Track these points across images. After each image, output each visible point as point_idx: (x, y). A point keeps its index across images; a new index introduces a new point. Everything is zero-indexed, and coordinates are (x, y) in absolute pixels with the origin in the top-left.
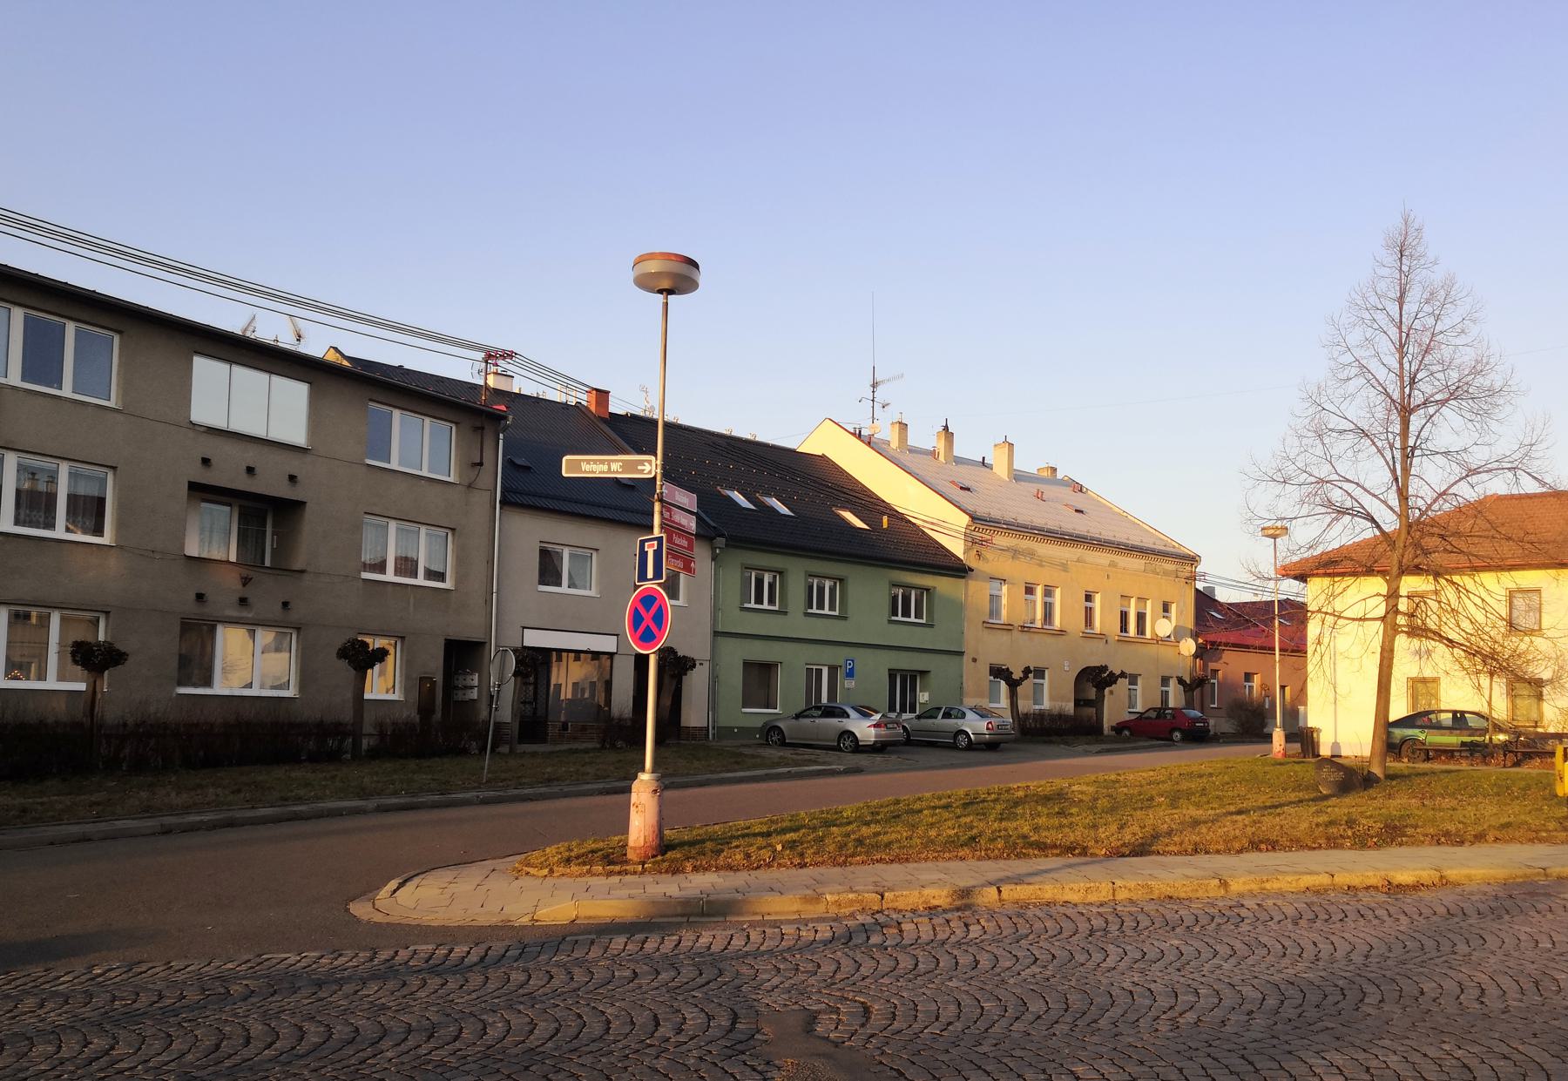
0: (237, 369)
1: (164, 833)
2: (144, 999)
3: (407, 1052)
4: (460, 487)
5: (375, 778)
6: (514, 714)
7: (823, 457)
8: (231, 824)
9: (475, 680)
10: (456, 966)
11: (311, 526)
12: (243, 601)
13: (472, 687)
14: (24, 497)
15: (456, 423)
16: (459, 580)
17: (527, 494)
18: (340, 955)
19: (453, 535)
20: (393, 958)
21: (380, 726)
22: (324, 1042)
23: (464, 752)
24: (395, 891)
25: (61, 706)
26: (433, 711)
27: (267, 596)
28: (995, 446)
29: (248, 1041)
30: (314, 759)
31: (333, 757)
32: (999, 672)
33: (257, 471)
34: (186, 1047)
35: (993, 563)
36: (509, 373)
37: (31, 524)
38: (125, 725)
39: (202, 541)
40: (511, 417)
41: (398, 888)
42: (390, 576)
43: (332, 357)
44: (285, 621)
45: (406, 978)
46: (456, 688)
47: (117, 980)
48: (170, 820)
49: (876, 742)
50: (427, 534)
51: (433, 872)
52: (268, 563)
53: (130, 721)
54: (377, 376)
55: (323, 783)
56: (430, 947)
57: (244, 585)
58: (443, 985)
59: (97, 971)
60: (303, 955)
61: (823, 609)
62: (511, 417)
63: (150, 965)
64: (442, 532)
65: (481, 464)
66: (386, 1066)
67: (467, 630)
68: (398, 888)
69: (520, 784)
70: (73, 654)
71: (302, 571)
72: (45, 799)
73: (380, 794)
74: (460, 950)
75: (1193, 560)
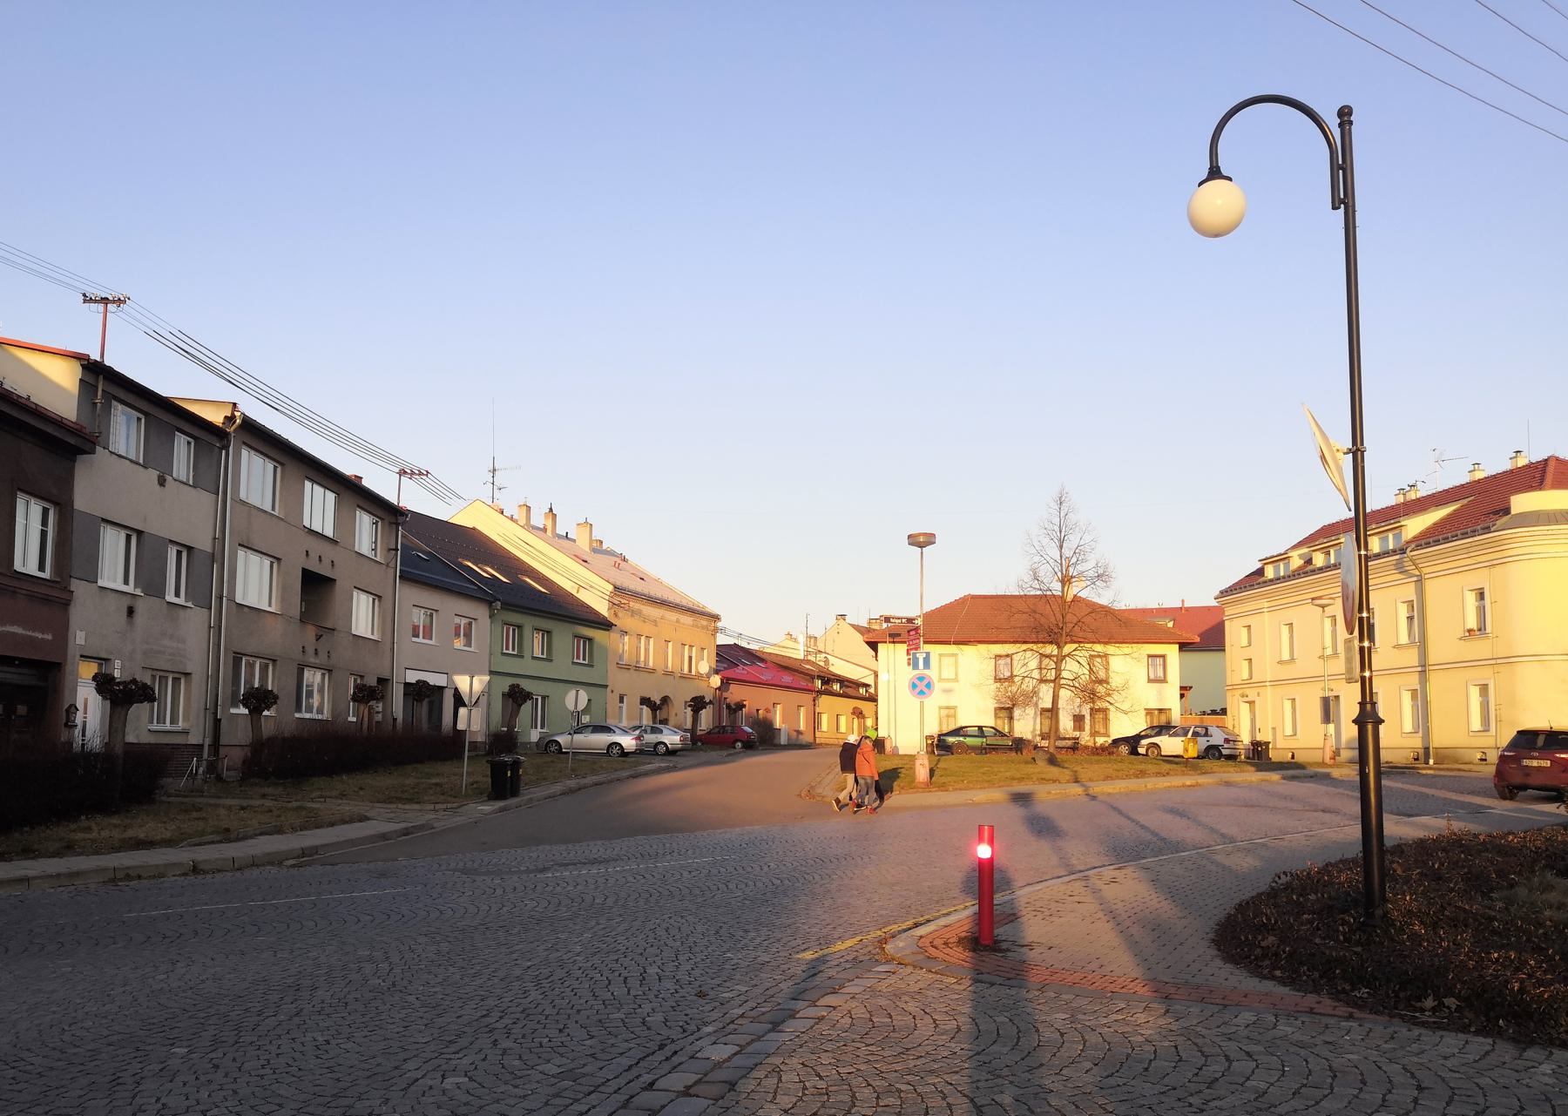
7: (474, 529)
15: (382, 519)
19: (379, 601)
28: (578, 525)
32: (645, 701)
35: (623, 621)
49: (636, 750)
67: (386, 675)
75: (716, 618)
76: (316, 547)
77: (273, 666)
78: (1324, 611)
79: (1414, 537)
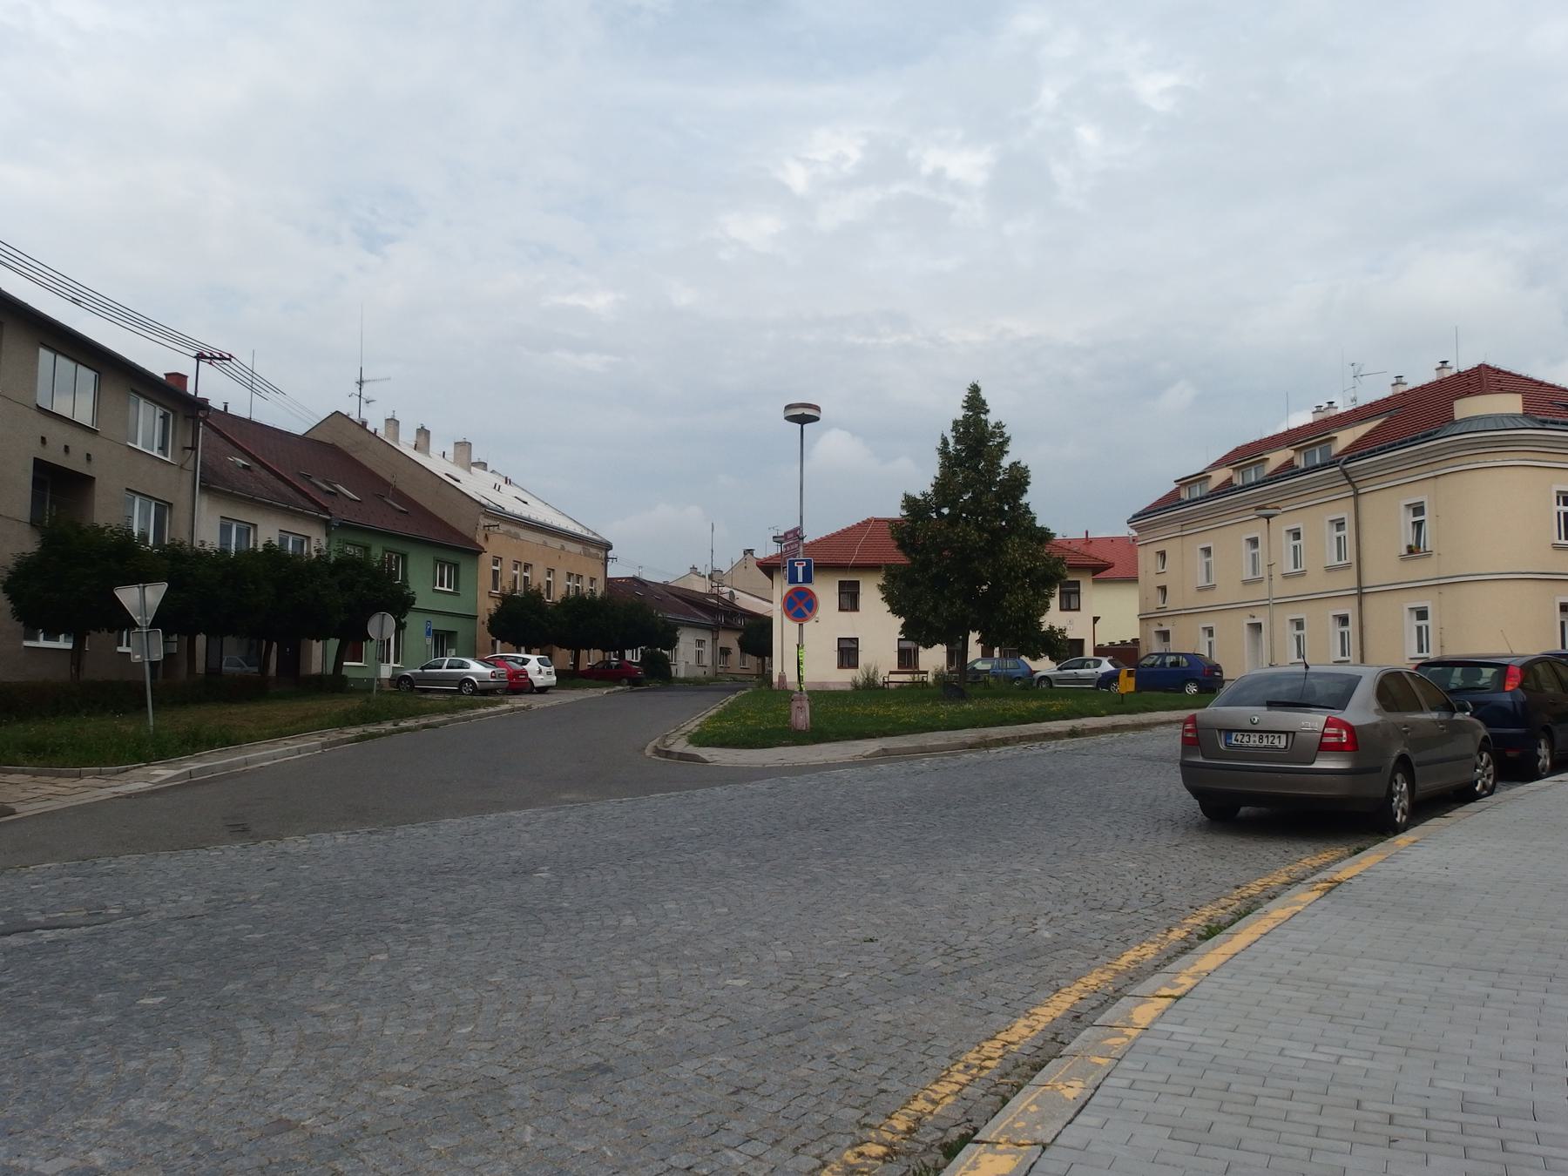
15: (173, 411)
61: (443, 586)
75: (608, 547)
76: (58, 434)
78: (1268, 522)
79: (1344, 450)
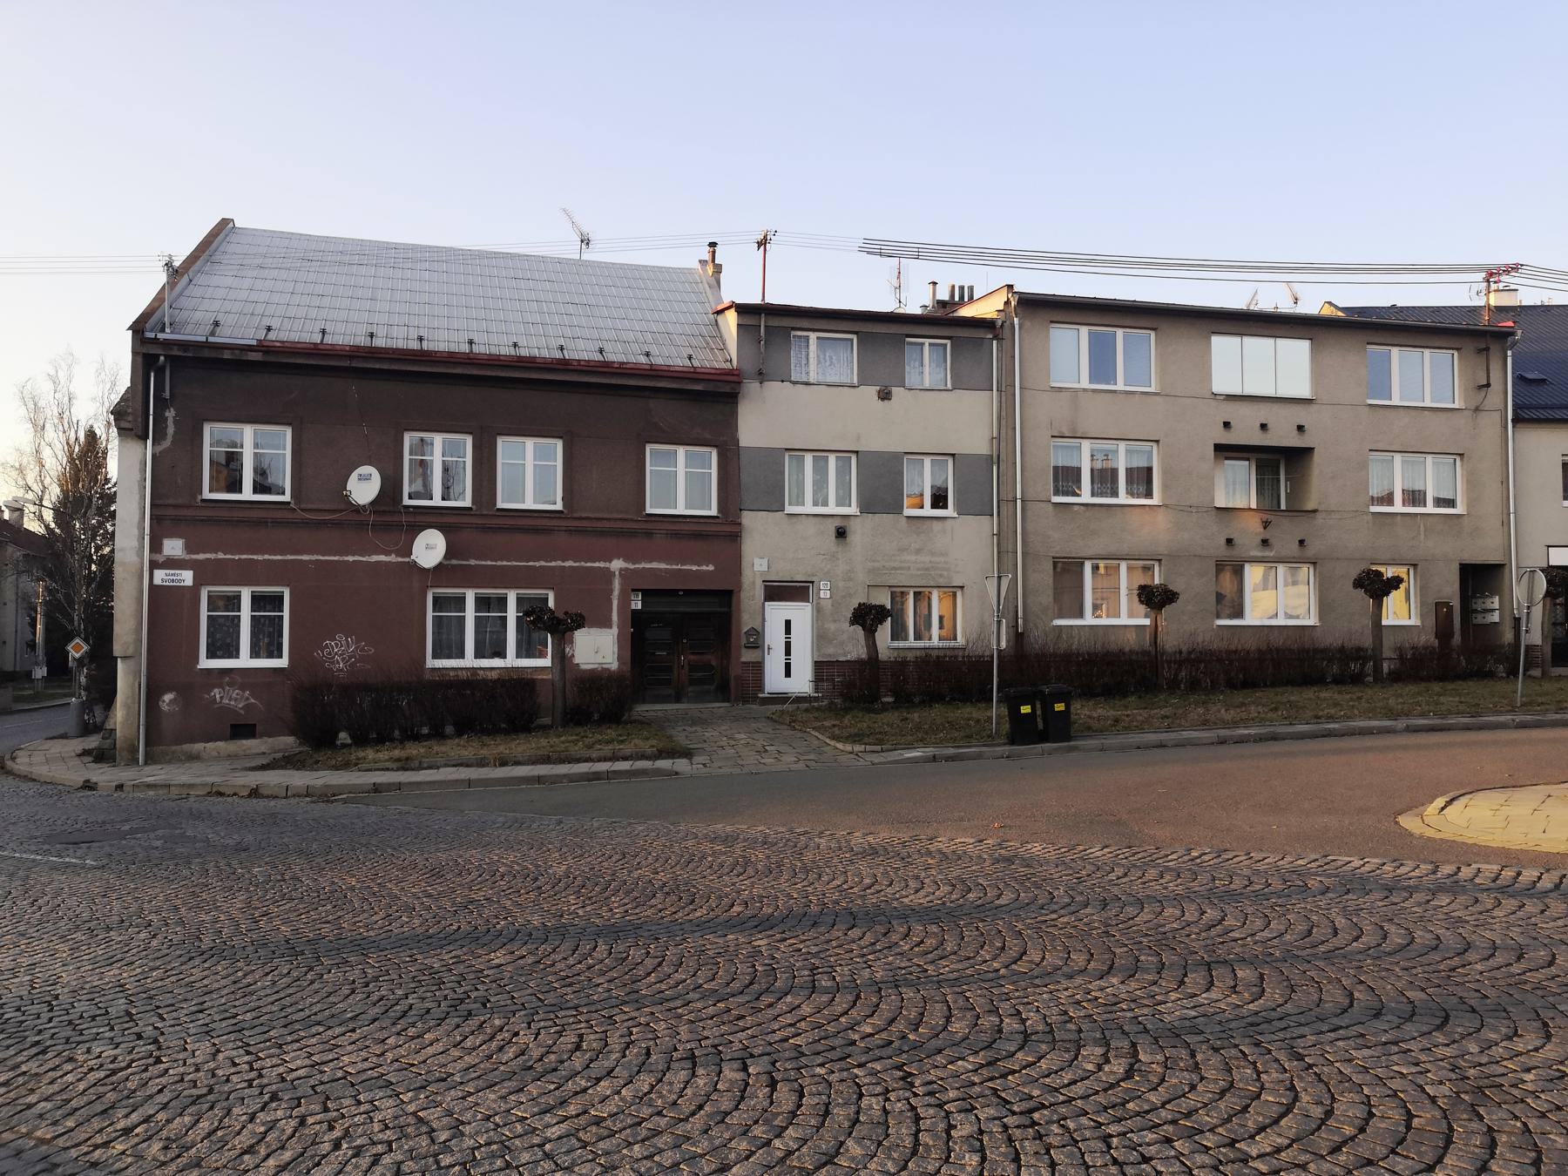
0: (1247, 340)
1: (1221, 743)
2: (1237, 884)
3: (1498, 969)
4: (1466, 412)
5: (1400, 700)
6: (1544, 637)
8: (1274, 738)
9: (1495, 602)
10: (1529, 890)
11: (1320, 470)
12: (1265, 542)
13: (1493, 610)
14: (1096, 473)
15: (1457, 349)
16: (1471, 503)
17: (1552, 408)
18: (1402, 865)
19: (1462, 460)
20: (1456, 874)
21: (1400, 650)
22: (1408, 945)
23: (1491, 675)
24: (1443, 809)
25: (1131, 637)
26: (1452, 635)
27: (1286, 535)
29: (1336, 933)
30: (1339, 681)
31: (1357, 680)
33: (1269, 426)
34: (1282, 928)
36: (1512, 287)
37: (1102, 495)
38: (1181, 652)
39: (1227, 493)
40: (1519, 332)
41: (1446, 806)
42: (1398, 507)
43: (1327, 312)
44: (1303, 555)
45: (1477, 895)
46: (1476, 611)
47: (1211, 863)
48: (1223, 732)
50: (1434, 463)
51: (1481, 794)
52: (1283, 507)
53: (1184, 649)
54: (1374, 319)
55: (1351, 703)
56: (1496, 868)
57: (1265, 528)
58: (1520, 907)
59: (1195, 854)
60: (1366, 860)
62: (1519, 332)
63: (1234, 854)
64: (1450, 459)
65: (1488, 385)
66: (1478, 977)
67: (1484, 551)
68: (1446, 806)
69: (1562, 709)
70: (1139, 595)
71: (1315, 511)
72: (1129, 712)
73: (1407, 715)
74: (1529, 875)
77: (1160, 566)
